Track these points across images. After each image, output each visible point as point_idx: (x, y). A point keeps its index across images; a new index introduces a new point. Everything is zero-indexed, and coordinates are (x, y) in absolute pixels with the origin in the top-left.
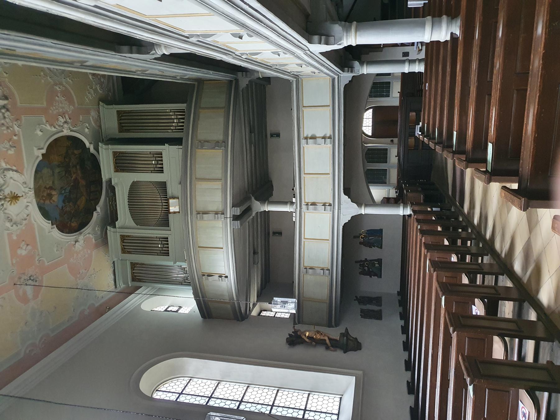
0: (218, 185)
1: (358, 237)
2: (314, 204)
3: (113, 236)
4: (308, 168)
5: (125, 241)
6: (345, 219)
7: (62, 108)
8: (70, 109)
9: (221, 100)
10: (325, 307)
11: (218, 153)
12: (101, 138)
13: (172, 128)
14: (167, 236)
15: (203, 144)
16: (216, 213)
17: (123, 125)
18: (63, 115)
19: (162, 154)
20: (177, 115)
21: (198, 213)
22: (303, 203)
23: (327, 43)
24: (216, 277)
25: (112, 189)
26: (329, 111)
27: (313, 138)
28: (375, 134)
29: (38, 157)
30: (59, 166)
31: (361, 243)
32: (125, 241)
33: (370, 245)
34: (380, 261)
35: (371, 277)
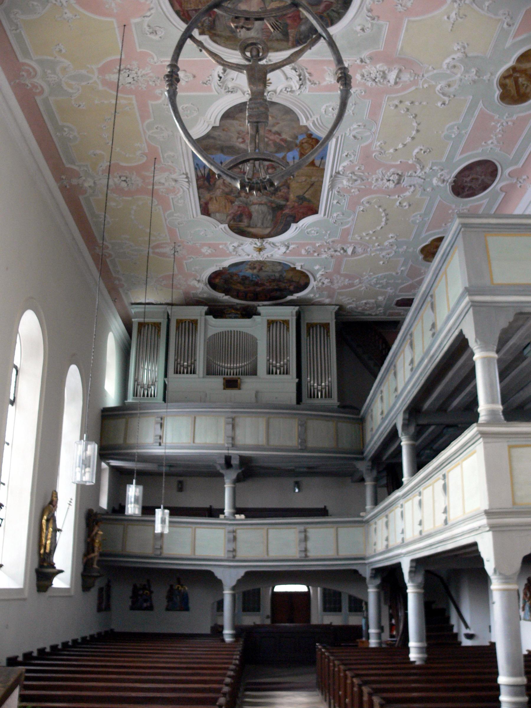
0: (262, 440)
1: (179, 582)
2: (235, 539)
3: (198, 312)
4: (273, 533)
5: (191, 324)
6: (219, 573)
7: (338, 282)
8: (336, 286)
9: (346, 443)
10: (118, 549)
11: (294, 442)
12: (303, 305)
13: (312, 382)
14: (197, 373)
15: (303, 426)
16: (233, 439)
17: (315, 328)
18: (331, 282)
19: (287, 374)
20: (325, 388)
21: (233, 419)
22: (235, 527)
23: (410, 572)
24: (159, 432)
25: (248, 313)
26: (331, 553)
27: (306, 539)
28: (276, 595)
29: (294, 265)
30: (281, 276)
31: (172, 586)
32: (191, 324)
33: (170, 597)
34: (150, 608)
35: (131, 598)
